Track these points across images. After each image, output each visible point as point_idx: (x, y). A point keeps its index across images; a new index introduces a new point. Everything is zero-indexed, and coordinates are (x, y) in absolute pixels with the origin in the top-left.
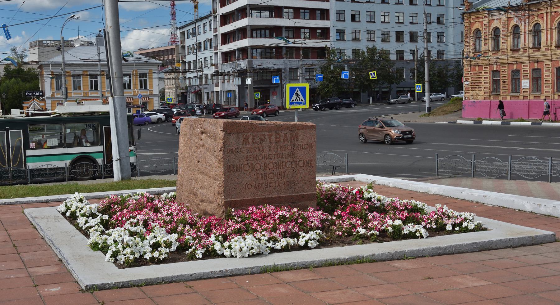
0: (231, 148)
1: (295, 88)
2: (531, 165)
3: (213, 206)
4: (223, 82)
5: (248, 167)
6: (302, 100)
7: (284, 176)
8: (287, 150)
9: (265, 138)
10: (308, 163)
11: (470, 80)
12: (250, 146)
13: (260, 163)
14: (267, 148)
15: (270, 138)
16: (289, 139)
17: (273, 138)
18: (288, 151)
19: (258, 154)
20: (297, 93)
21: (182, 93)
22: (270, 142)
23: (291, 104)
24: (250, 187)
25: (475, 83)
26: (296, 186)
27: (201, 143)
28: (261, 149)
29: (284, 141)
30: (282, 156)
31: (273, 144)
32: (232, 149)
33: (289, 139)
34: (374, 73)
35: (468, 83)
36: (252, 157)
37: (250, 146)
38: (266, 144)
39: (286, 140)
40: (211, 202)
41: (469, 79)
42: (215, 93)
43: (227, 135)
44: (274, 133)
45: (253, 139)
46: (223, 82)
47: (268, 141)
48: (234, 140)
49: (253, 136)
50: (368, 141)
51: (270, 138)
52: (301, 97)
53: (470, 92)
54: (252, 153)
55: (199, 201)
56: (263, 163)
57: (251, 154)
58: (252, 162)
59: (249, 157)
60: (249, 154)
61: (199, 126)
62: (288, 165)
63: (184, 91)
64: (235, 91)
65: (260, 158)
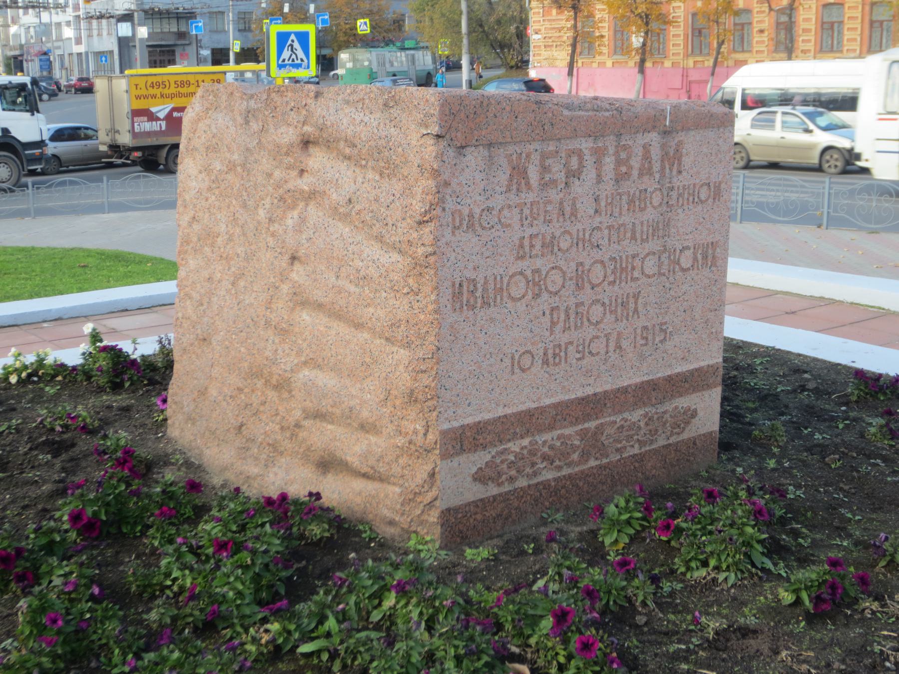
0: (466, 212)
1: (288, 34)
2: (786, 191)
3: (377, 443)
4: (90, 36)
5: (522, 284)
6: (302, 60)
7: (636, 311)
8: (650, 209)
9: (581, 166)
10: (705, 257)
11: (543, 31)
12: (531, 197)
13: (561, 263)
14: (586, 207)
15: (598, 163)
16: (656, 167)
17: (609, 162)
18: (650, 215)
19: (556, 228)
20: (292, 46)
21: (15, 57)
22: (599, 179)
23: (280, 67)
24: (526, 361)
25: (550, 38)
26: (669, 345)
27: (304, 184)
28: (568, 209)
29: (641, 175)
30: (634, 232)
31: (608, 188)
32: (471, 215)
33: (656, 167)
34: (365, 23)
35: (539, 36)
36: (538, 243)
37: (531, 197)
38: (582, 188)
39: (646, 171)
40: (365, 427)
41: (540, 30)
42: (75, 58)
43: (451, 152)
44: (610, 142)
45: (545, 169)
46: (90, 36)
47: (590, 174)
48: (479, 176)
49: (544, 157)
50: (752, 163)
51: (598, 163)
52: (300, 53)
53: (543, 52)
54: (540, 227)
55: (298, 414)
56: (573, 265)
57: (534, 230)
58: (539, 263)
59: (526, 243)
60: (529, 231)
61: (293, 117)
62: (650, 266)
63: (17, 53)
64: (112, 52)
65: (564, 245)
